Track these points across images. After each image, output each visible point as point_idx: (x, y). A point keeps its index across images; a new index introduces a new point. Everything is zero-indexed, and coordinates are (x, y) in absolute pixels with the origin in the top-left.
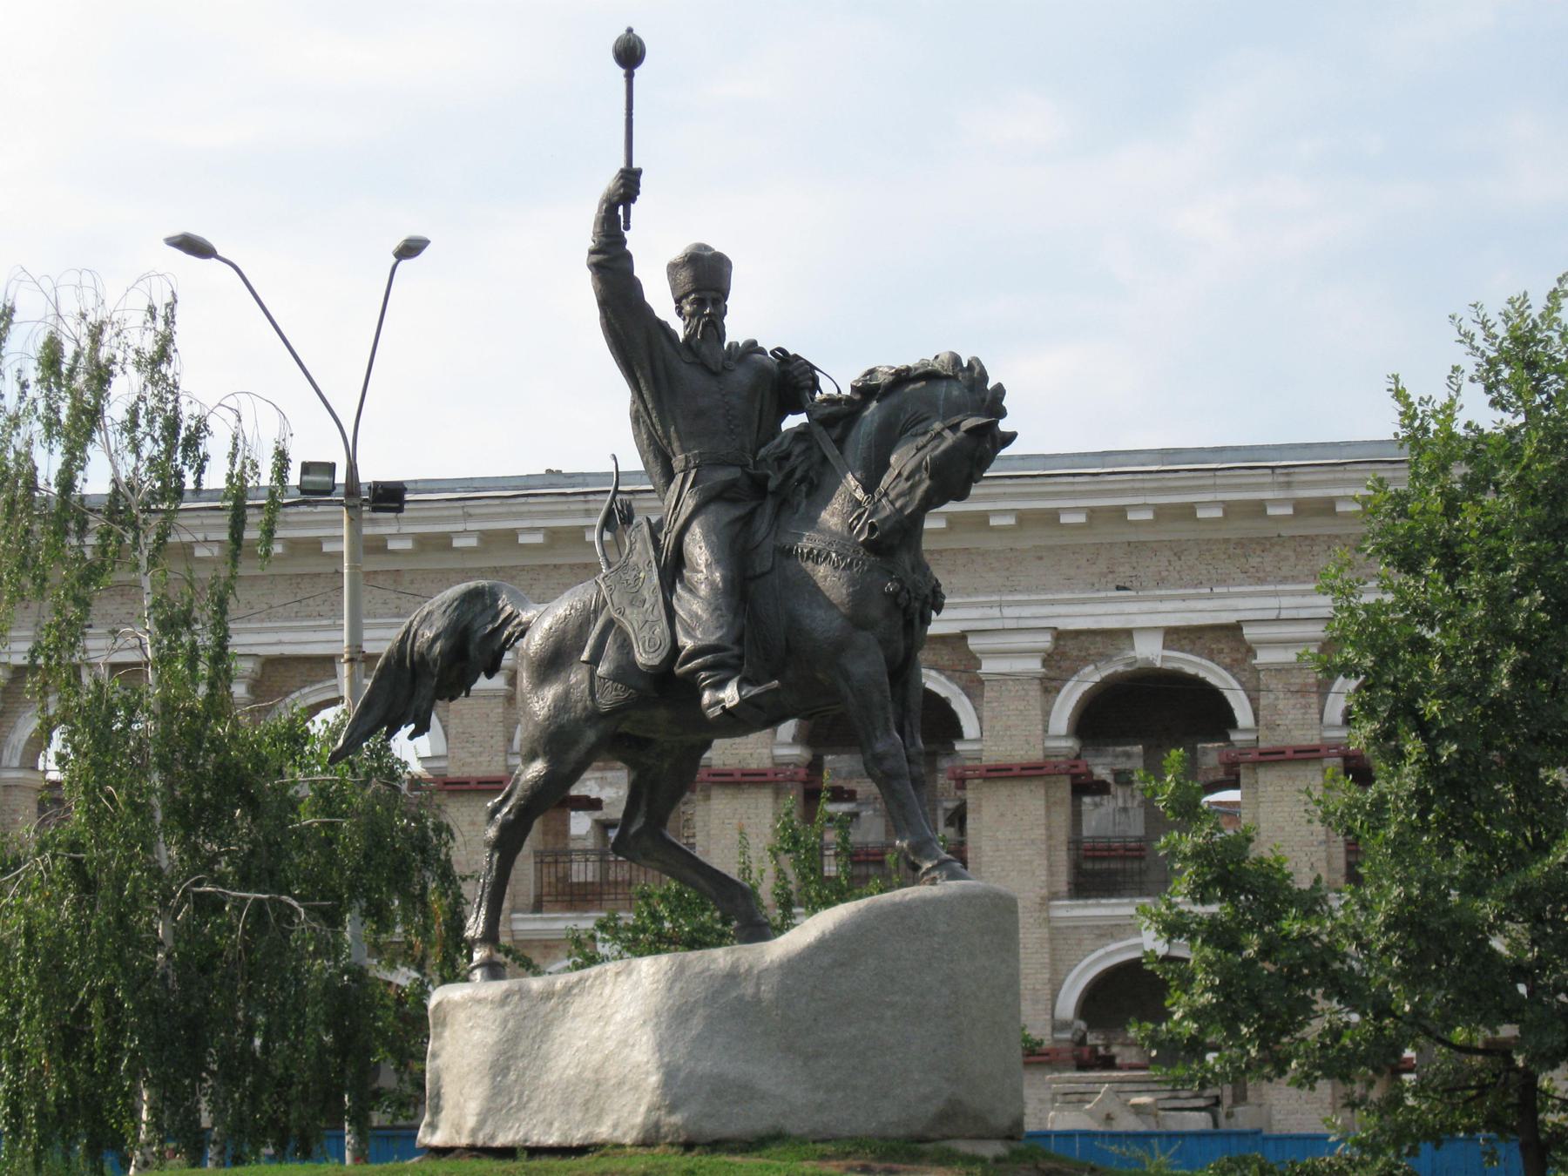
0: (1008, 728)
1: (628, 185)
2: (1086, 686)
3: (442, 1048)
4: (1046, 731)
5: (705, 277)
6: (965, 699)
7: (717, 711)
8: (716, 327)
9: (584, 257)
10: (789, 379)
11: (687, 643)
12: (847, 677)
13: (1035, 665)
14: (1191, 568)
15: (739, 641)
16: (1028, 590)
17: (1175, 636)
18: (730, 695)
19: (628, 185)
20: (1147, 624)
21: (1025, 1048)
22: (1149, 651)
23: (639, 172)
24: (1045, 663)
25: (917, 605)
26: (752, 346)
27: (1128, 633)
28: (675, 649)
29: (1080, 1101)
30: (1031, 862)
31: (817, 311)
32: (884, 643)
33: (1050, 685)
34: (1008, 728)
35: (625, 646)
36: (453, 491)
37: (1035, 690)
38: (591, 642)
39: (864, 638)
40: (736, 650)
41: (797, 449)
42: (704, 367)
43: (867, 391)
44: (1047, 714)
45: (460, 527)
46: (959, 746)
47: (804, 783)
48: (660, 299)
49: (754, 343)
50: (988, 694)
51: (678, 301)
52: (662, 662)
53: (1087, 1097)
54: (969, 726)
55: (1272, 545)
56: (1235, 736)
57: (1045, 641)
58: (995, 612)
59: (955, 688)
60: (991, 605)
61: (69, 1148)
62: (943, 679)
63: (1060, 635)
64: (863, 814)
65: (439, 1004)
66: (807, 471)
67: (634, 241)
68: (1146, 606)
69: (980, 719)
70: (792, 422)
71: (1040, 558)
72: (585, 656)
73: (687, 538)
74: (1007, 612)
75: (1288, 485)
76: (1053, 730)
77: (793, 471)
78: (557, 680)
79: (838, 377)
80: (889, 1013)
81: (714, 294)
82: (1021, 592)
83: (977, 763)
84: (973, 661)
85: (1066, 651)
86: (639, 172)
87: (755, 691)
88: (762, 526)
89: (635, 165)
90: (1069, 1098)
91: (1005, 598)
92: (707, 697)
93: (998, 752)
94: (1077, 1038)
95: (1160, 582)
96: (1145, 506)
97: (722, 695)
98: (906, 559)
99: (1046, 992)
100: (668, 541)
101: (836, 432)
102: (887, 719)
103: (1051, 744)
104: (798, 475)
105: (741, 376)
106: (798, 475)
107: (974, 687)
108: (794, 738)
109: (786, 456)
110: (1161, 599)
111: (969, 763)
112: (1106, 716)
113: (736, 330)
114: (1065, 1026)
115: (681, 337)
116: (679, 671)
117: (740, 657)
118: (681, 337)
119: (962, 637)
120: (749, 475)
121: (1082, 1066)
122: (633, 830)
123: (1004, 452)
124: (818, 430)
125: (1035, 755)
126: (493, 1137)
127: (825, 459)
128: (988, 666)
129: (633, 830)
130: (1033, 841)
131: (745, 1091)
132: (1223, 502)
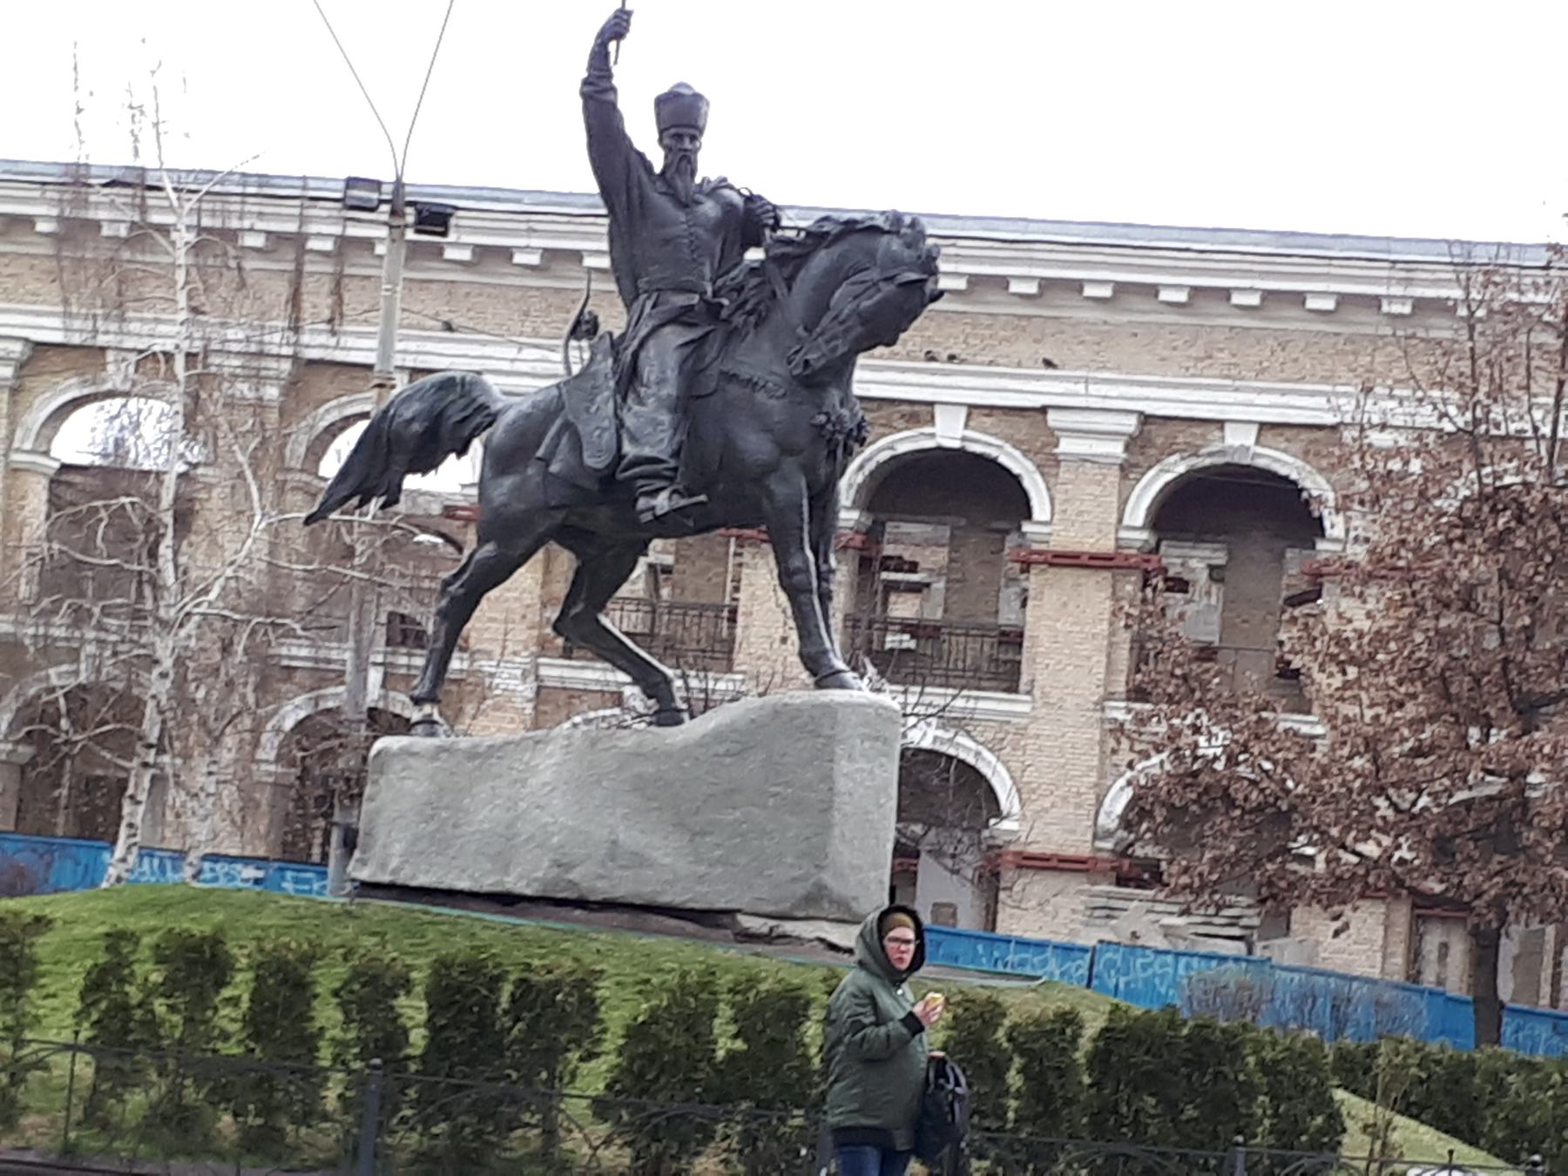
0: (1080, 513)
1: (617, 27)
2: (1169, 477)
3: (378, 793)
4: (1120, 520)
5: (681, 117)
6: (1038, 477)
7: (647, 517)
8: (689, 162)
9: (578, 85)
10: (750, 220)
11: (629, 449)
12: (770, 495)
13: (1117, 449)
14: (1296, 360)
15: (676, 454)
16: (1118, 369)
17: (1266, 428)
18: (662, 502)
19: (617, 27)
20: (1243, 413)
21: (898, 844)
22: (1239, 443)
23: (629, 14)
24: (1127, 448)
25: (840, 437)
26: (723, 183)
27: (1220, 423)
28: (619, 456)
29: (1108, 917)
30: (1089, 658)
31: (783, 156)
32: (809, 470)
33: (1129, 470)
34: (1080, 513)
35: (577, 446)
36: (519, 201)
37: (1114, 475)
38: (547, 441)
39: (789, 464)
40: (672, 463)
41: (754, 281)
42: (673, 195)
43: (817, 238)
44: (1123, 503)
45: (522, 242)
46: (1027, 527)
47: (861, 549)
48: (643, 133)
49: (725, 180)
50: (1064, 474)
51: (661, 132)
52: (607, 467)
53: (1116, 913)
54: (1040, 509)
55: (1386, 345)
56: (1321, 545)
57: (1130, 424)
58: (1081, 388)
59: (1030, 466)
60: (1077, 380)
61: (389, 1147)
62: (1017, 454)
63: (1146, 419)
64: (934, 586)
65: (379, 753)
66: (758, 303)
67: (621, 76)
68: (1241, 397)
69: (1052, 500)
70: (754, 255)
71: (1135, 335)
72: (540, 453)
73: (643, 355)
74: (1093, 389)
75: (1409, 282)
76: (1126, 521)
77: (745, 302)
78: (515, 472)
79: (794, 223)
80: (771, 802)
81: (692, 131)
82: (1109, 369)
83: (1043, 547)
84: (1053, 437)
85: (1150, 437)
86: (629, 14)
87: (683, 502)
88: (712, 350)
89: (628, 7)
90: (1097, 913)
91: (1092, 374)
92: (642, 503)
93: (1065, 538)
94: (1119, 849)
95: (1260, 373)
96: (1252, 289)
97: (654, 502)
98: (834, 395)
99: (1091, 798)
100: (627, 356)
101: (787, 272)
102: (802, 540)
103: (1123, 534)
104: (748, 307)
105: (709, 209)
106: (748, 307)
107: (1049, 463)
108: (854, 502)
109: (740, 289)
110: (1261, 391)
111: (1035, 547)
112: (1182, 511)
113: (708, 166)
114: (1109, 834)
115: (658, 169)
116: (621, 476)
117: (675, 469)
118: (658, 169)
119: (1043, 410)
120: (706, 302)
121: (1121, 881)
122: (573, 612)
123: (932, 306)
124: (771, 266)
125: (1107, 545)
126: (413, 877)
127: (774, 294)
128: (1066, 446)
129: (573, 612)
130: (1094, 636)
131: (640, 860)
132: (1338, 294)
